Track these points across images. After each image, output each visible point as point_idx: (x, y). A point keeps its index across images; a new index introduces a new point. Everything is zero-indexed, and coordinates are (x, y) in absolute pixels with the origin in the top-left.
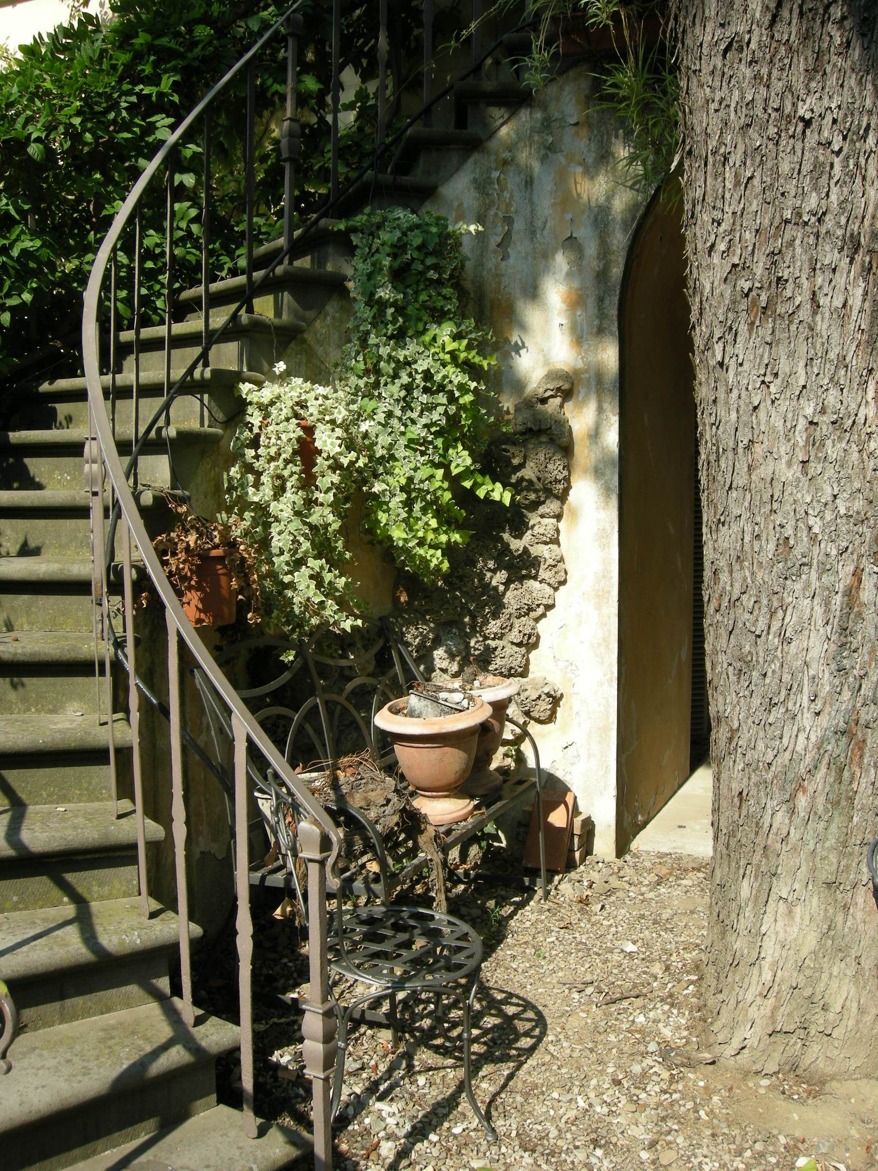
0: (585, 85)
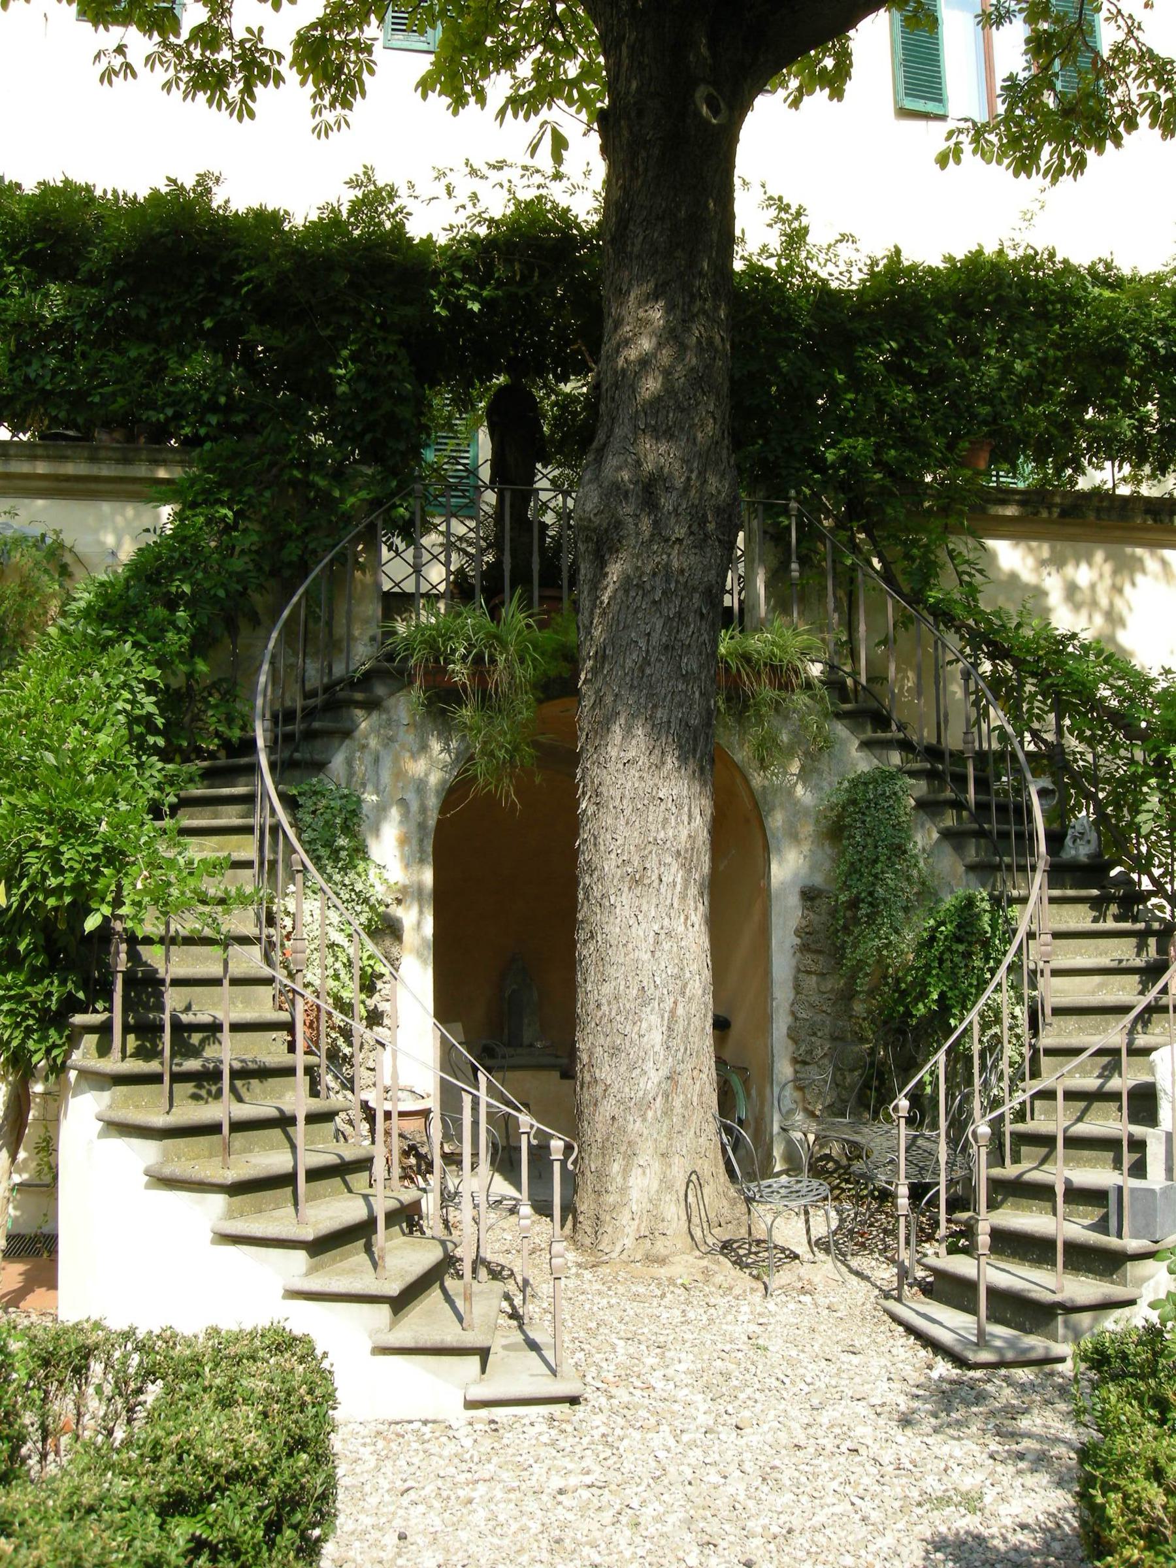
0: (818, 880)
